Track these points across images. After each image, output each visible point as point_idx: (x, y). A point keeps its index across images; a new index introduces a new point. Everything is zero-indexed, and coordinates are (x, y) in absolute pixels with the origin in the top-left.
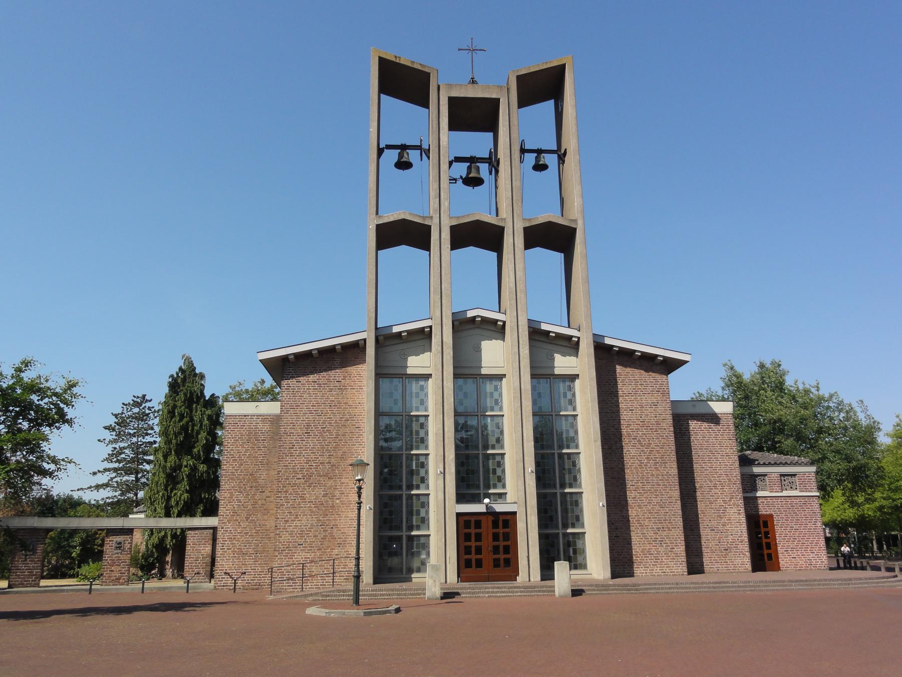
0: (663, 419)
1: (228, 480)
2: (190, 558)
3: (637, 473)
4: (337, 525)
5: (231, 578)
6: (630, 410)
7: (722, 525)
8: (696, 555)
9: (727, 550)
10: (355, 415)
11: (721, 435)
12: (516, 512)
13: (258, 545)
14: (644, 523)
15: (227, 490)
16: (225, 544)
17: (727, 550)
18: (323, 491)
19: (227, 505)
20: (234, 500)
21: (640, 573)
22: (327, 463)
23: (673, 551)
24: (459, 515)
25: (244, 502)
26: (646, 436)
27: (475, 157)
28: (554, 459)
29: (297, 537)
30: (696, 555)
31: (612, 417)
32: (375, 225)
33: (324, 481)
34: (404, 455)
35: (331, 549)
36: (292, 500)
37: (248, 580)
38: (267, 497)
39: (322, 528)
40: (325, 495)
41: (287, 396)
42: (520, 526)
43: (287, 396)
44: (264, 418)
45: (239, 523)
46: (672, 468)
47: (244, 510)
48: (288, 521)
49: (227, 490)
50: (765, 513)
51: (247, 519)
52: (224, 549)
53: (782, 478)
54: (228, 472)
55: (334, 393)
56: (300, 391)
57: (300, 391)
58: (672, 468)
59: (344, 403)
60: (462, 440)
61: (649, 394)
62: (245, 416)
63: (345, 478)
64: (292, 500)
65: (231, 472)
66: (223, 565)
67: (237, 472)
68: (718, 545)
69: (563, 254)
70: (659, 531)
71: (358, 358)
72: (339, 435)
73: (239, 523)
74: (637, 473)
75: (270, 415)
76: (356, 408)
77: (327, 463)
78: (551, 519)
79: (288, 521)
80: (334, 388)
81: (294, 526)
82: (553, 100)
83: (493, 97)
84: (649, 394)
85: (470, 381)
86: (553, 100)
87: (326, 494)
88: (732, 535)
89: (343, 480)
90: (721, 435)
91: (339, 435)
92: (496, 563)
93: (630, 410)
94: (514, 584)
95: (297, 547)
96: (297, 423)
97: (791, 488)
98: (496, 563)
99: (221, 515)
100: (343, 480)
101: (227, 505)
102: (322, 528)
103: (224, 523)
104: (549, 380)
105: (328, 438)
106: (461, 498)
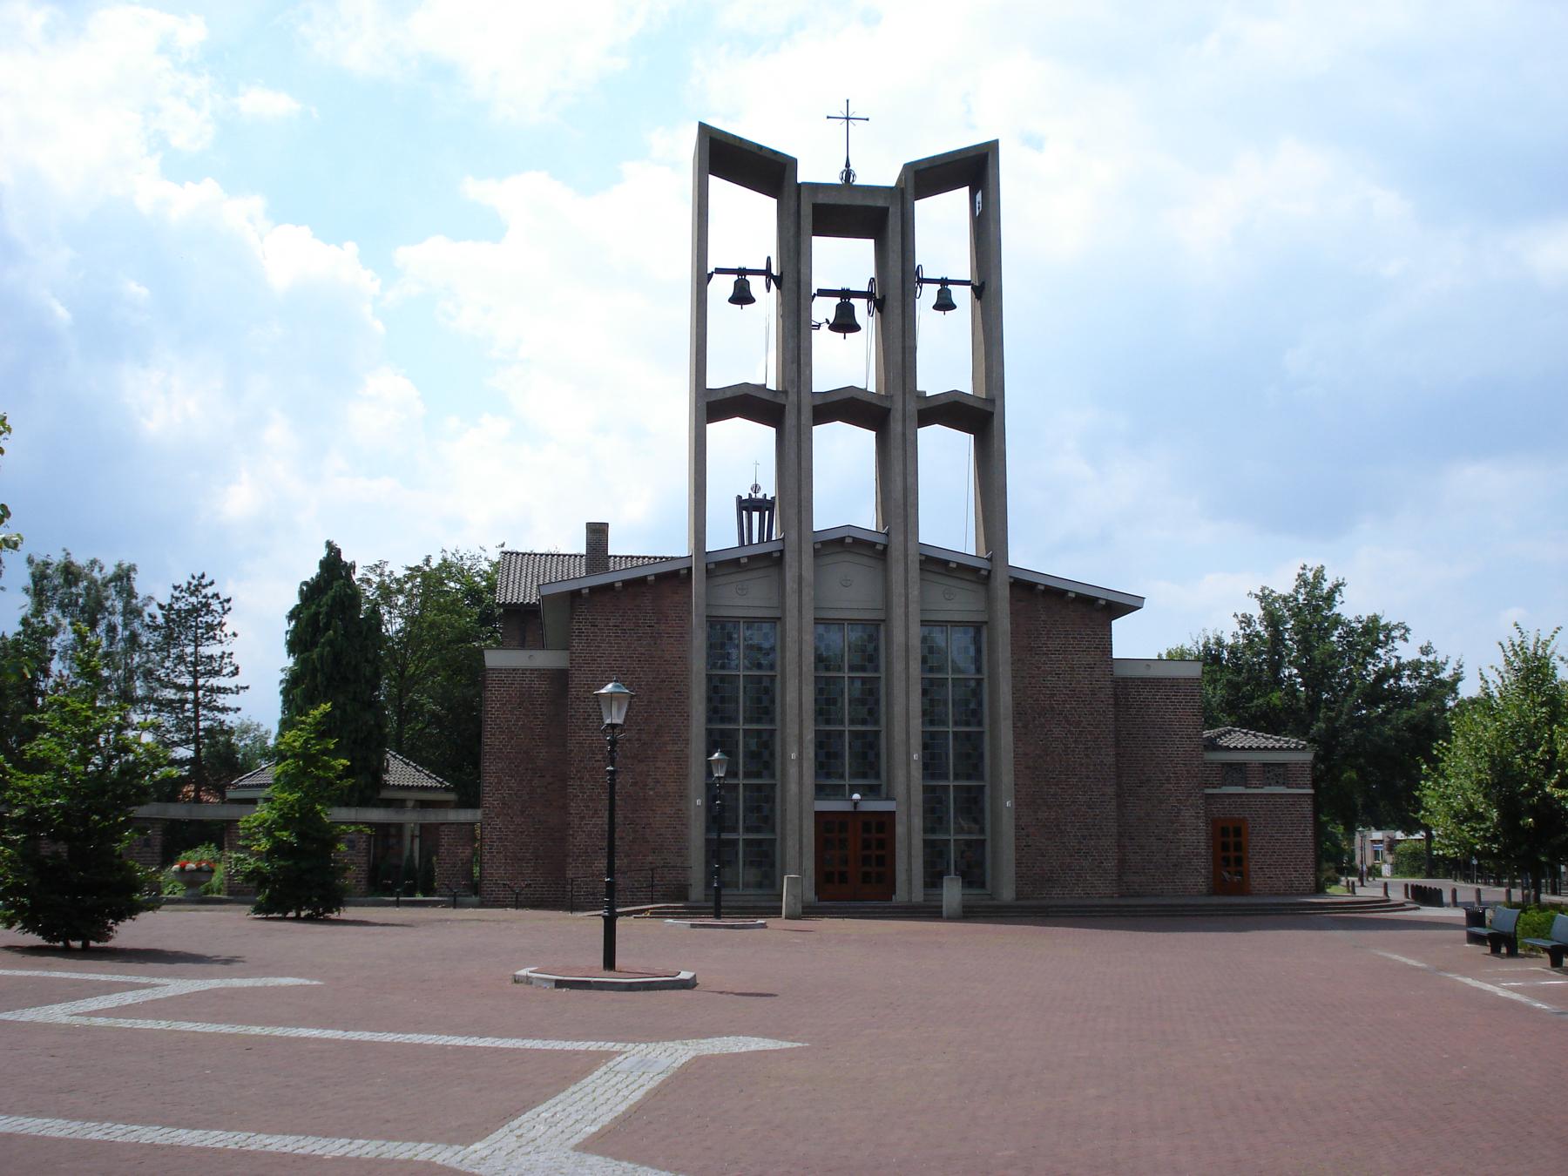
0: (1100, 688)
1: (494, 759)
2: (445, 863)
3: (1061, 761)
4: (650, 824)
5: (513, 891)
6: (1056, 674)
7: (1173, 833)
8: (1134, 873)
9: (1176, 865)
10: (674, 675)
11: (1182, 709)
12: (894, 812)
13: (539, 849)
14: (1065, 829)
15: (494, 773)
16: (493, 845)
17: (1176, 865)
18: (631, 778)
19: (494, 794)
20: (502, 787)
21: (1055, 894)
22: (637, 740)
23: (1100, 867)
24: (819, 814)
25: (518, 790)
26: (1076, 711)
27: (848, 290)
28: (947, 738)
29: (597, 838)
30: (1134, 873)
31: (1030, 684)
32: (705, 403)
33: (632, 765)
34: (741, 731)
35: (644, 856)
36: (589, 789)
37: (527, 894)
38: (549, 784)
39: (631, 828)
40: (634, 784)
41: (578, 646)
42: (900, 830)
43: (578, 646)
44: (542, 673)
45: (512, 818)
46: (1108, 755)
47: (517, 801)
48: (584, 817)
49: (494, 773)
50: (594, 1129)
51: (522, 812)
52: (492, 852)
53: (1267, 769)
54: (493, 748)
55: (645, 642)
56: (596, 640)
57: (596, 640)
58: (1108, 755)
59: (659, 657)
60: (711, 644)
61: (1083, 651)
62: (514, 670)
63: (661, 761)
64: (589, 789)
65: (497, 749)
66: (492, 873)
67: (506, 749)
68: (1165, 859)
69: (972, 436)
70: (1085, 839)
71: (677, 593)
72: (652, 702)
73: (512, 818)
74: (1061, 761)
75: (548, 670)
76: (675, 664)
77: (637, 740)
78: (940, 819)
79: (584, 817)
80: (644, 635)
81: (593, 824)
82: (968, 187)
83: (878, 205)
84: (1083, 651)
85: (834, 628)
86: (968, 187)
87: (637, 782)
88: (1185, 846)
89: (659, 764)
90: (1182, 709)
91: (652, 702)
92: (866, 877)
93: (1056, 674)
94: (887, 904)
95: (597, 852)
96: (594, 684)
97: (1277, 782)
98: (866, 877)
99: (486, 807)
100: (659, 764)
101: (494, 794)
102: (631, 828)
103: (491, 818)
104: (945, 628)
105: (637, 706)
106: (821, 791)
